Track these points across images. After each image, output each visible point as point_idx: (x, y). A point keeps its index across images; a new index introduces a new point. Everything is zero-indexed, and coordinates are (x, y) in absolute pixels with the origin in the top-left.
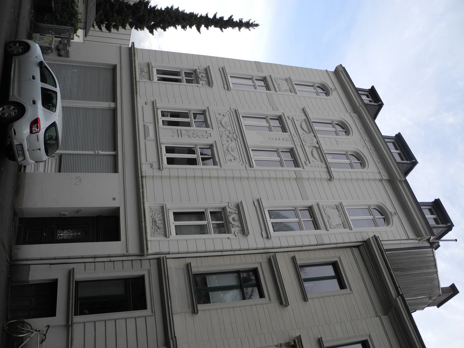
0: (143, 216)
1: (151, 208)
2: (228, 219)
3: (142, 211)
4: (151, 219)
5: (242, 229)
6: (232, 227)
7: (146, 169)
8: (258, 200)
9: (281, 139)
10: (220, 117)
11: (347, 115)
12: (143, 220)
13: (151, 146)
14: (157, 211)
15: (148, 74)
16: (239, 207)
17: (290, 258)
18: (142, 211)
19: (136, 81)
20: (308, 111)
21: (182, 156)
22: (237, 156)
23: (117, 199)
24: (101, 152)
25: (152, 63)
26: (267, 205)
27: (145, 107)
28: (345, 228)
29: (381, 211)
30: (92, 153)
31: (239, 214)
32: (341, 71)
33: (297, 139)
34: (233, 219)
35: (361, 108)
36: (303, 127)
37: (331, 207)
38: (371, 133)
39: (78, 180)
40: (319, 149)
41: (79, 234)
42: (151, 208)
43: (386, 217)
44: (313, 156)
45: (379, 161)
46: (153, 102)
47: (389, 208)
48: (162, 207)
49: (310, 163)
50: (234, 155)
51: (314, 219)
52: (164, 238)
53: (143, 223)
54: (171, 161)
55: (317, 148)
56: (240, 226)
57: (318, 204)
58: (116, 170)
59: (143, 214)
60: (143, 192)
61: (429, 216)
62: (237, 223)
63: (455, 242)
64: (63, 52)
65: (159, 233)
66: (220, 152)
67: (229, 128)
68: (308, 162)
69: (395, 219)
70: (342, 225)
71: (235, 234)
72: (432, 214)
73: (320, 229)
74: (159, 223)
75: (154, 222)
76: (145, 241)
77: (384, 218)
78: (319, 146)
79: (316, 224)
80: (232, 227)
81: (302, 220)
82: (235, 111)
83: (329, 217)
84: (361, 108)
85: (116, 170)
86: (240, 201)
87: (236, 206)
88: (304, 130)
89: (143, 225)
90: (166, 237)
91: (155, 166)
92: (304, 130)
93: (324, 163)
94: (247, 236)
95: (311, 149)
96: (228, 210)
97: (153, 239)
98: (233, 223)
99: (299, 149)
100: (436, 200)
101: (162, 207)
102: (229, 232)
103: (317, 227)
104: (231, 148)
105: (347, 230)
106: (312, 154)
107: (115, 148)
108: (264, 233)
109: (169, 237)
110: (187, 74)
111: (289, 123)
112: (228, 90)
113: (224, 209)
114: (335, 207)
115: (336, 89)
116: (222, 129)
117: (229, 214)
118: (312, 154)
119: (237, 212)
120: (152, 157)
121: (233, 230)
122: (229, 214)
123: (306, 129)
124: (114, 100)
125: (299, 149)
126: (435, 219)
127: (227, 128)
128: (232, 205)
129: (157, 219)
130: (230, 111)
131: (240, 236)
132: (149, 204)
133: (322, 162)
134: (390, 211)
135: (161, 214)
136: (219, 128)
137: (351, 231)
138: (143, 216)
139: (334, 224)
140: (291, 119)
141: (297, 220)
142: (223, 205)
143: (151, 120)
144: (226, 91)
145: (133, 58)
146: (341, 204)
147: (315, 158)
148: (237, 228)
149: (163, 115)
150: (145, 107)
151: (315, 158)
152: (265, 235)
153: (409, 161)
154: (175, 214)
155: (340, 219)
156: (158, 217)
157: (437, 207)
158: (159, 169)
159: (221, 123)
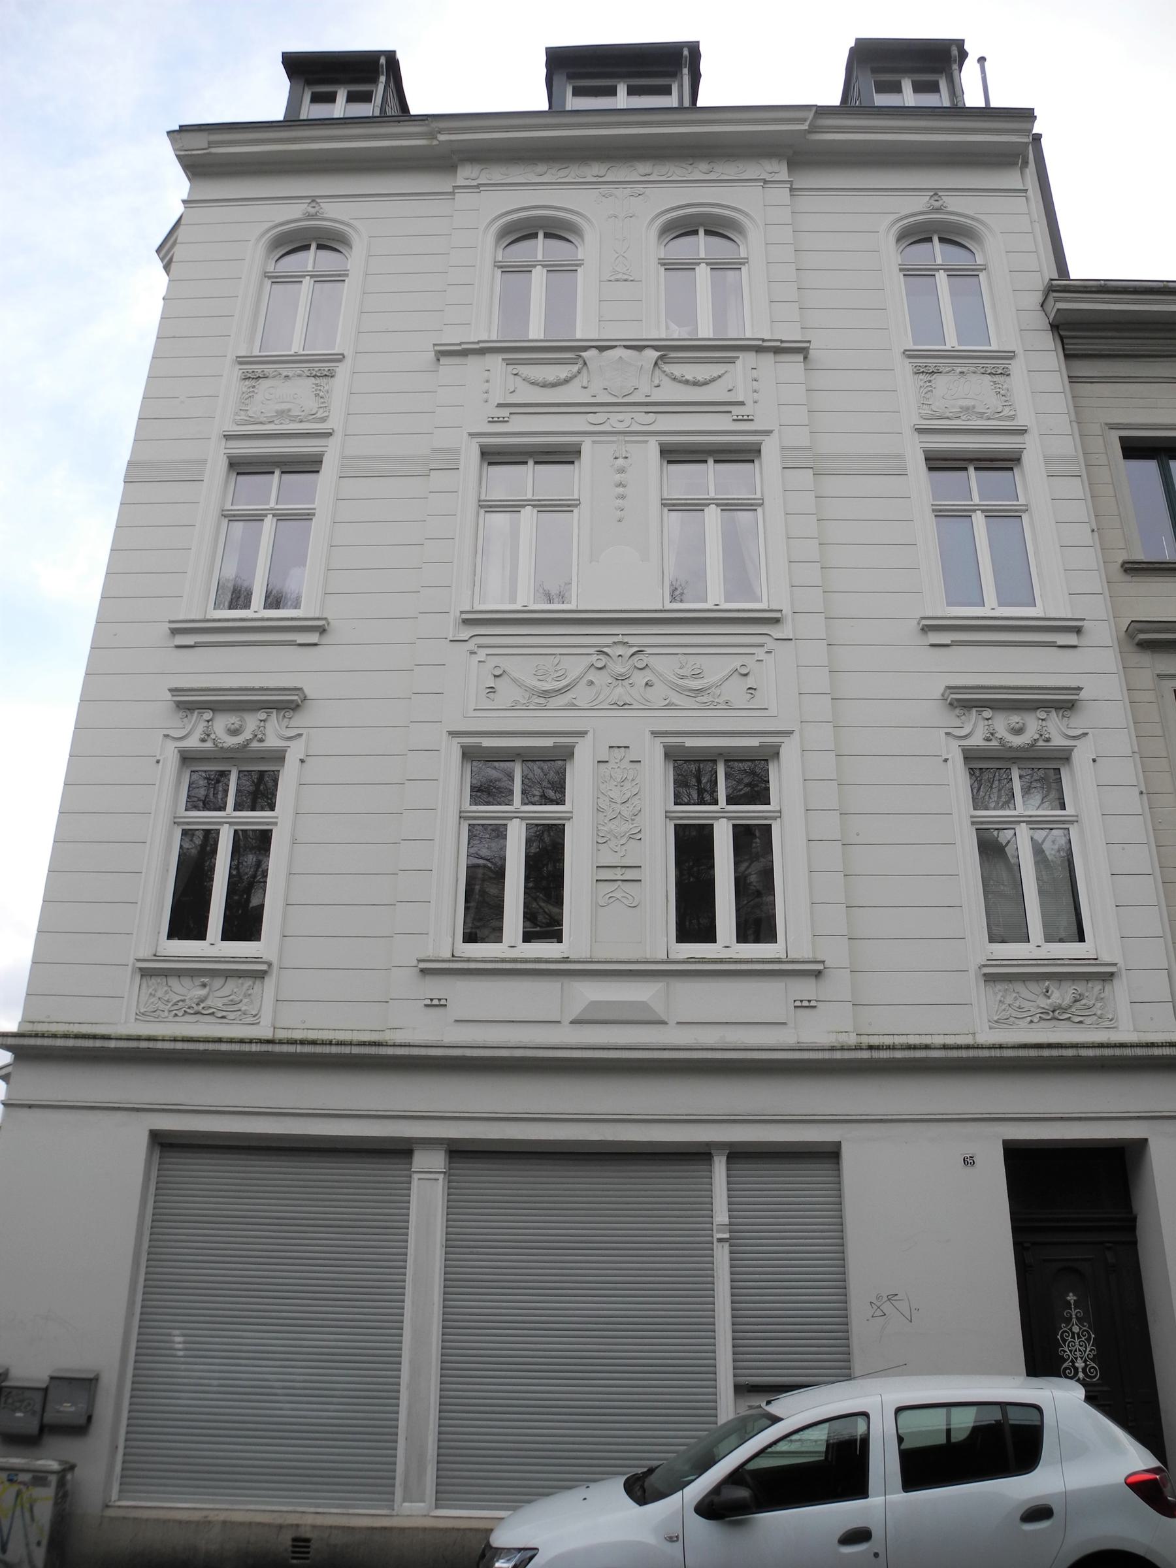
0: (1054, 1053)
1: (141, 1016)
2: (230, 749)
3: (1033, 1053)
4: (188, 1018)
5: (1057, 709)
6: (1048, 740)
7: (822, 1030)
8: (174, 632)
9: (618, 477)
10: (508, 693)
11: (653, 192)
12: (1070, 1052)
13: (469, 997)
14: (159, 994)
15: (217, 983)
16: (189, 704)
17: (1128, 578)
18: (1033, 1053)
19: (858, 1048)
20: (453, 337)
21: (721, 879)
22: (736, 662)
23: (969, 1152)
24: (721, 1216)
25: (141, 956)
26: (199, 605)
27: (456, 1010)
28: (330, 375)
29: (293, 242)
30: (722, 1255)
31: (217, 708)
32: (211, 144)
33: (621, 417)
34: (234, 732)
35: (442, 137)
36: (551, 379)
37: (250, 396)
38: (788, 143)
39: (887, 1307)
40: (667, 352)
41: (1071, 1298)
42: (141, 1016)
43: (314, 239)
44: (706, 383)
45: (704, 166)
46: (423, 971)
47: (290, 214)
48: (146, 973)
49: (742, 403)
50: (726, 672)
51: (971, 460)
52: (270, 983)
53: (1084, 1052)
54: (757, 924)
55: (661, 357)
56: (262, 715)
57: (228, 437)
58: (830, 1154)
59: (1046, 1053)
60: (945, 1047)
61: (340, 108)
62: (251, 722)
63: (986, 64)
64: (67, 1407)
65: (247, 995)
66: (716, 726)
67: (575, 667)
68: (736, 410)
69: (335, 213)
70: (318, 381)
71: (1074, 738)
72: (331, 98)
73: (1020, 451)
74: (1061, 995)
75: (1054, 1014)
76: (277, 1048)
77: (320, 247)
78: (656, 348)
79: (992, 460)
80: (1048, 740)
81: (272, 504)
82: (467, 622)
83: (283, 412)
84: (442, 137)
85: (830, 1154)
86: (169, 696)
87: (181, 714)
88: (566, 381)
89: (1090, 1053)
90: (265, 972)
91: (805, 989)
92: (566, 381)
93: (741, 355)
94: (305, 699)
95: (666, 382)
96: (193, 742)
97: (266, 1019)
98: (247, 735)
99: (666, 423)
100: (853, 52)
101: (146, 973)
102: (279, 757)
103: (310, 465)
104: (683, 677)
105: (342, 370)
106: (696, 384)
107: (699, 1155)
108: (1062, 639)
109: (270, 964)
110: (206, 794)
111: (519, 424)
112: (322, 630)
113: (187, 758)
114: (247, 383)
115: (313, 199)
116: (582, 695)
117: (994, 743)
118: (696, 384)
119: (208, 715)
120: (770, 999)
121: (1058, 741)
122: (994, 743)
123: (563, 372)
124: (399, 1151)
125: (666, 423)
126: (352, 98)
127: (572, 676)
128: (178, 725)
129: (1044, 1003)
130: (471, 645)
131: (299, 720)
132: (982, 1023)
133: (731, 361)
134: (298, 215)
135: (1019, 987)
136: (572, 707)
137: (348, 361)
138: (1054, 1053)
139: (311, 404)
140: (505, 412)
141: (269, 521)
142: (957, 757)
143: (548, 988)
144: (326, 639)
145: (112, 1044)
146: (241, 361)
147: (713, 380)
148: (268, 725)
149: (708, 935)
150: (456, 1010)
151: (713, 380)
152: (313, 638)
153: (363, 74)
154: (684, 935)
155: (974, 378)
156: (1032, 998)
157: (309, 71)
158: (818, 974)
159: (546, 694)
